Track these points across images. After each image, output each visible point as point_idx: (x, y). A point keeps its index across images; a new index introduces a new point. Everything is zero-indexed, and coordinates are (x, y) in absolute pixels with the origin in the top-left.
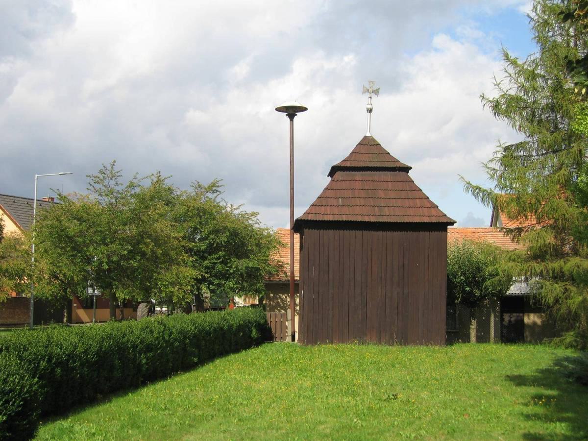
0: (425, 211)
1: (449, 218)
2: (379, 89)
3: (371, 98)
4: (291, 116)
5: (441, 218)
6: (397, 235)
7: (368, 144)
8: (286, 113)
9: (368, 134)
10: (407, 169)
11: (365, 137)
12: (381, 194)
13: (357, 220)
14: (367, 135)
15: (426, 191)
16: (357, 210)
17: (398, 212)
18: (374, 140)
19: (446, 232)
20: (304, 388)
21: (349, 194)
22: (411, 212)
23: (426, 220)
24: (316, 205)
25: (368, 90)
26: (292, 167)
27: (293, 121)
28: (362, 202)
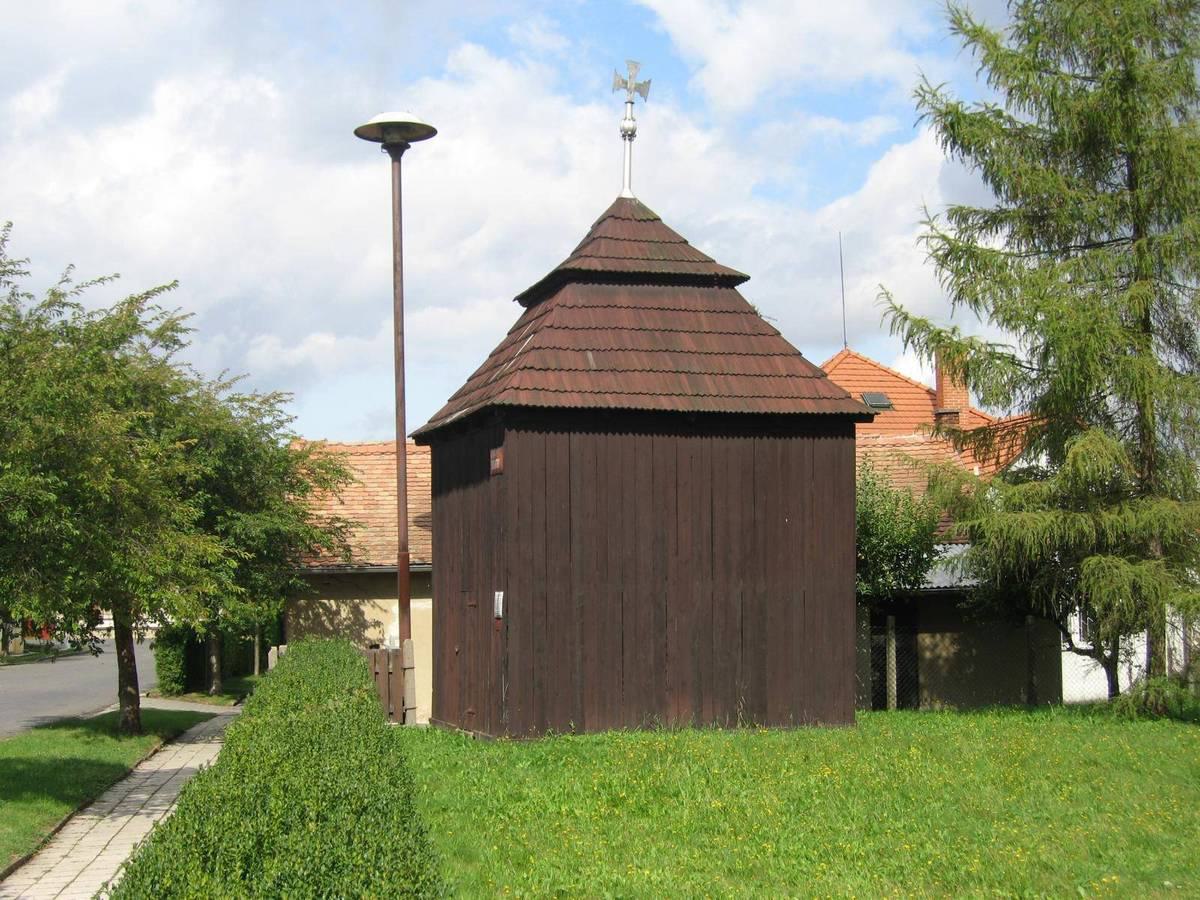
0: (803, 387)
2: (650, 81)
3: (632, 103)
4: (396, 150)
5: (842, 403)
6: (738, 443)
7: (627, 217)
9: (627, 194)
10: (733, 280)
11: (621, 201)
12: (687, 342)
13: (645, 408)
14: (624, 196)
16: (638, 382)
17: (738, 386)
18: (644, 209)
19: (852, 439)
21: (608, 339)
22: (769, 387)
24: (532, 368)
25: (626, 83)
26: (398, 278)
27: (400, 161)
28: (646, 361)
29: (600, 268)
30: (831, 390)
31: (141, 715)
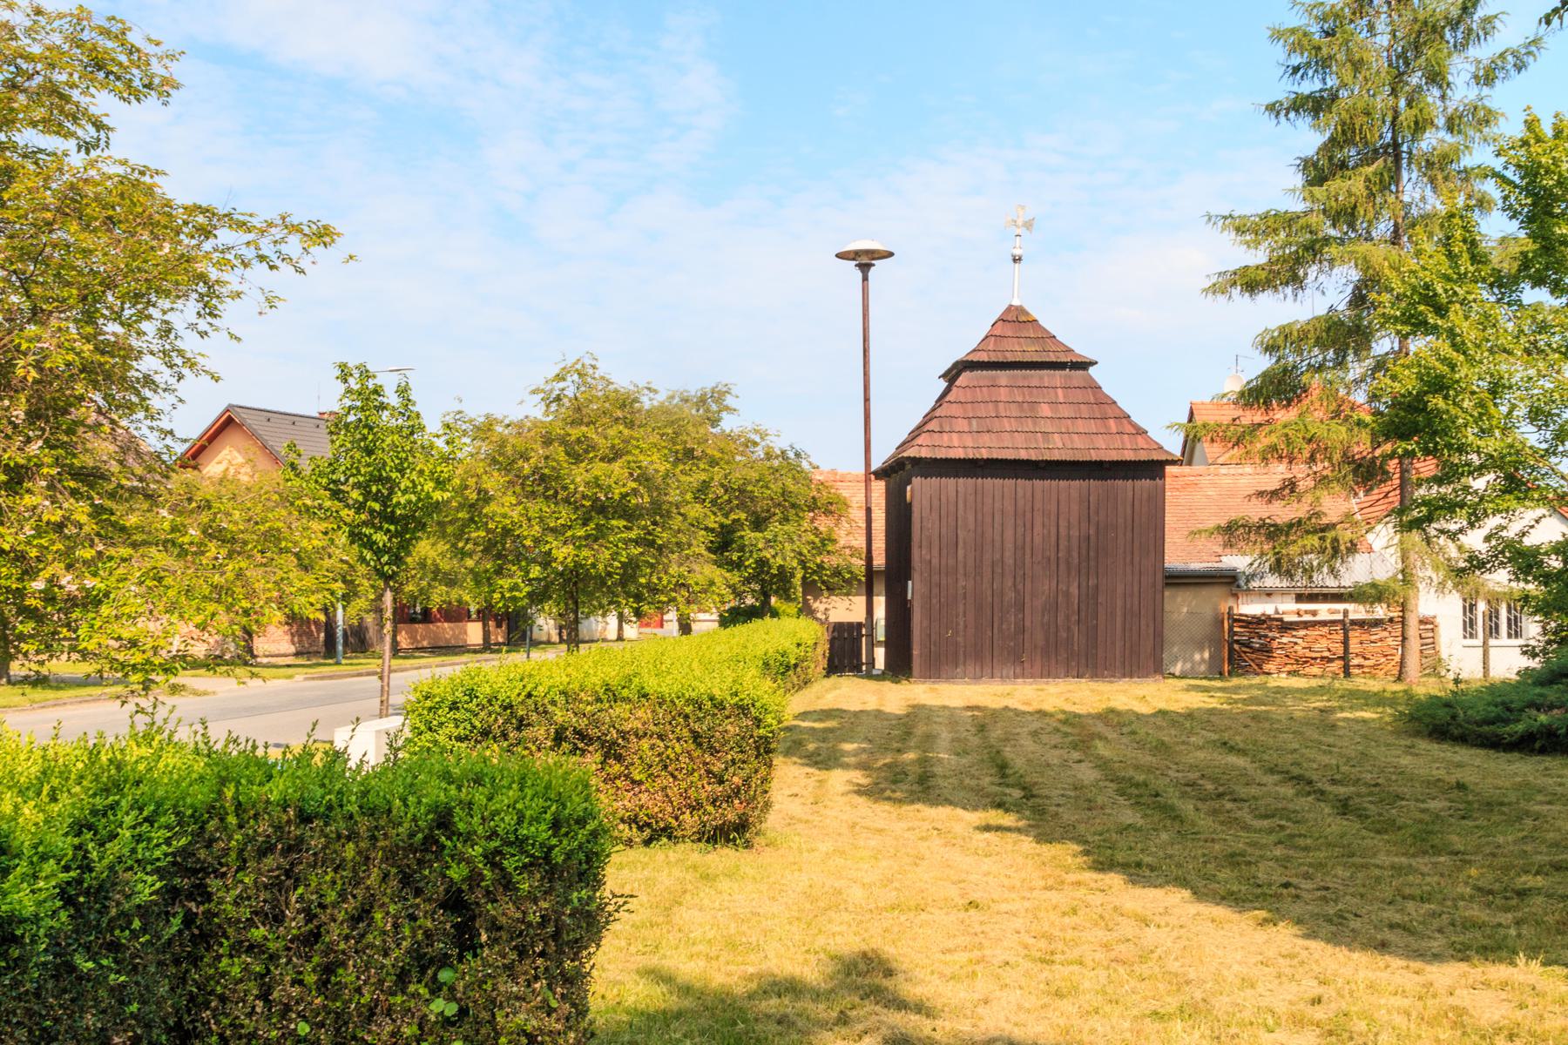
1: (1167, 452)
4: (865, 268)
6: (1076, 486)
7: (1016, 319)
8: (855, 263)
9: (1016, 302)
10: (1084, 365)
11: (1010, 308)
15: (1124, 404)
17: (1078, 442)
20: (1436, 160)
23: (1129, 456)
28: (1014, 425)
29: (986, 360)
30: (1148, 443)
31: (864, 590)
